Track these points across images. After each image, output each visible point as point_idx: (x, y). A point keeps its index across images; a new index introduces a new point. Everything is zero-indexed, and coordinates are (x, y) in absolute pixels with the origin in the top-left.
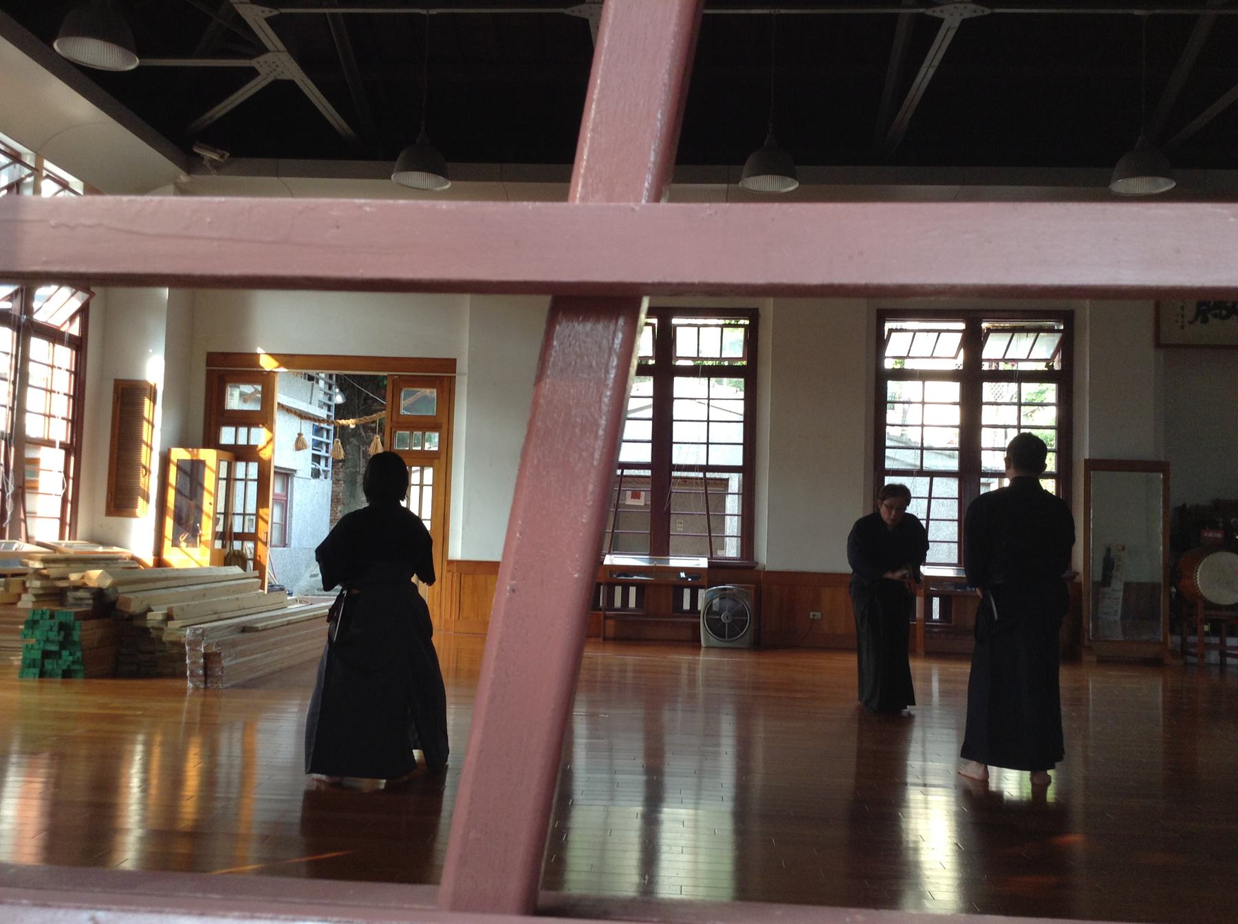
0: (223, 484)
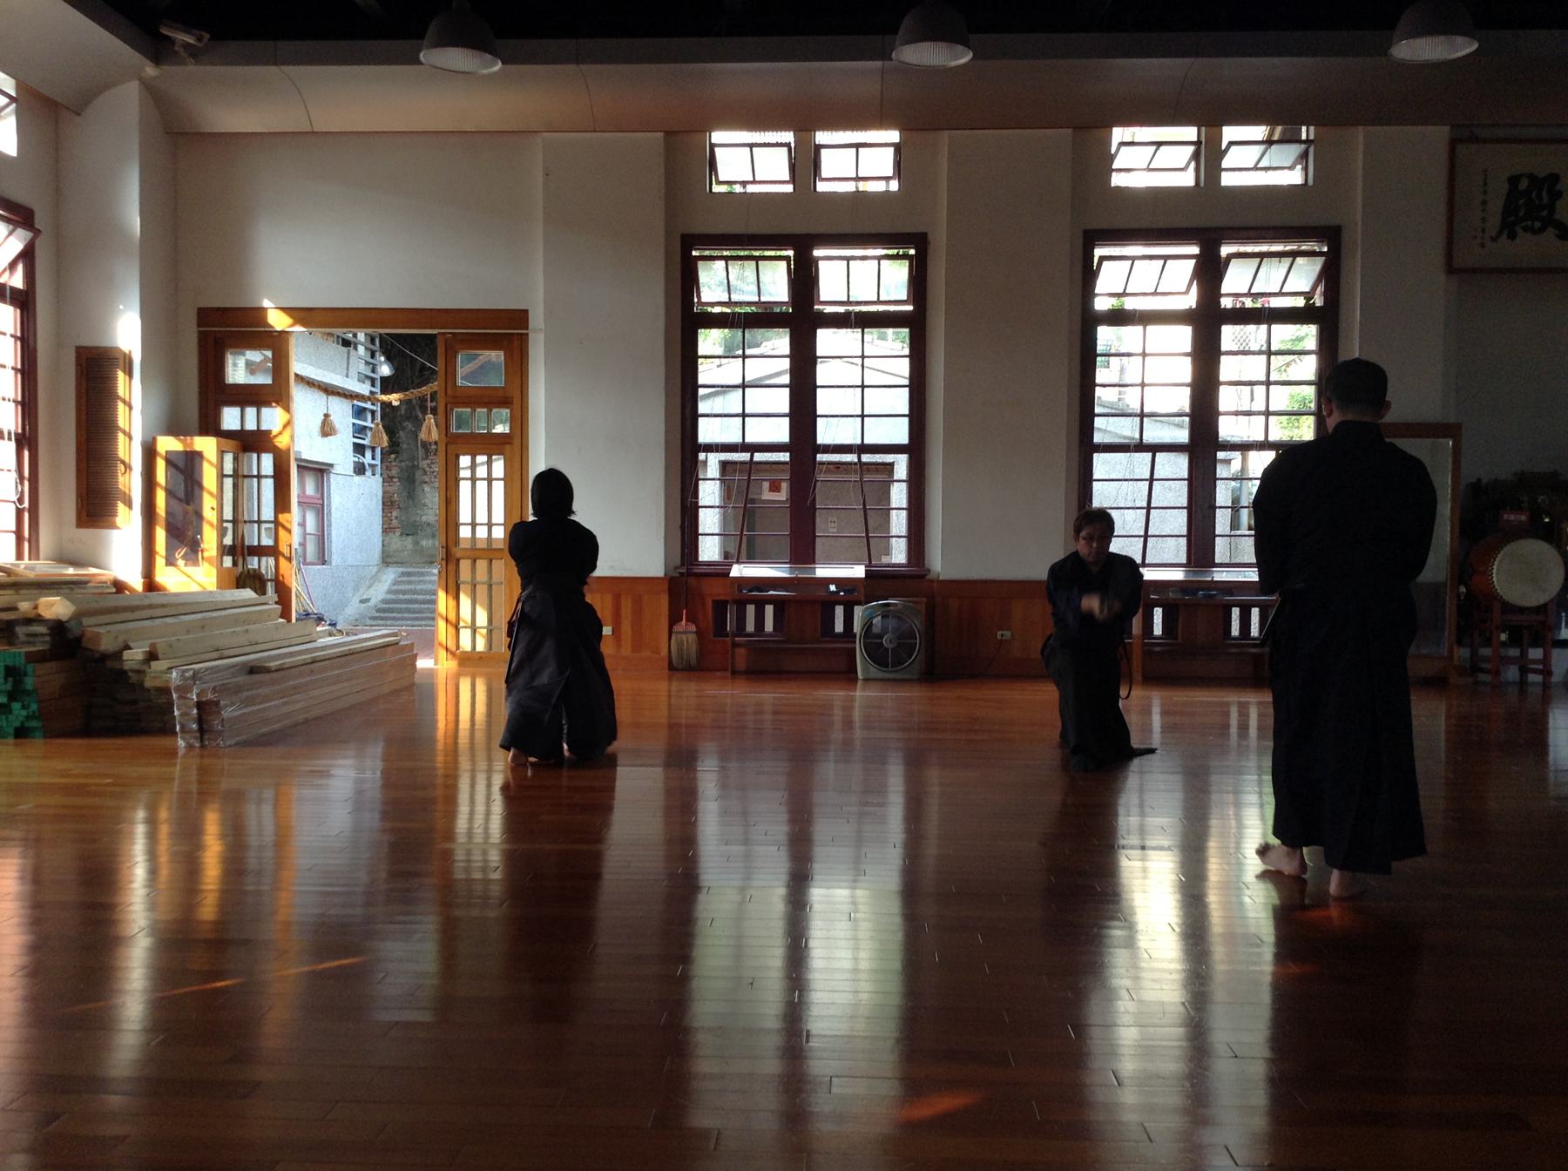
0: (228, 483)
